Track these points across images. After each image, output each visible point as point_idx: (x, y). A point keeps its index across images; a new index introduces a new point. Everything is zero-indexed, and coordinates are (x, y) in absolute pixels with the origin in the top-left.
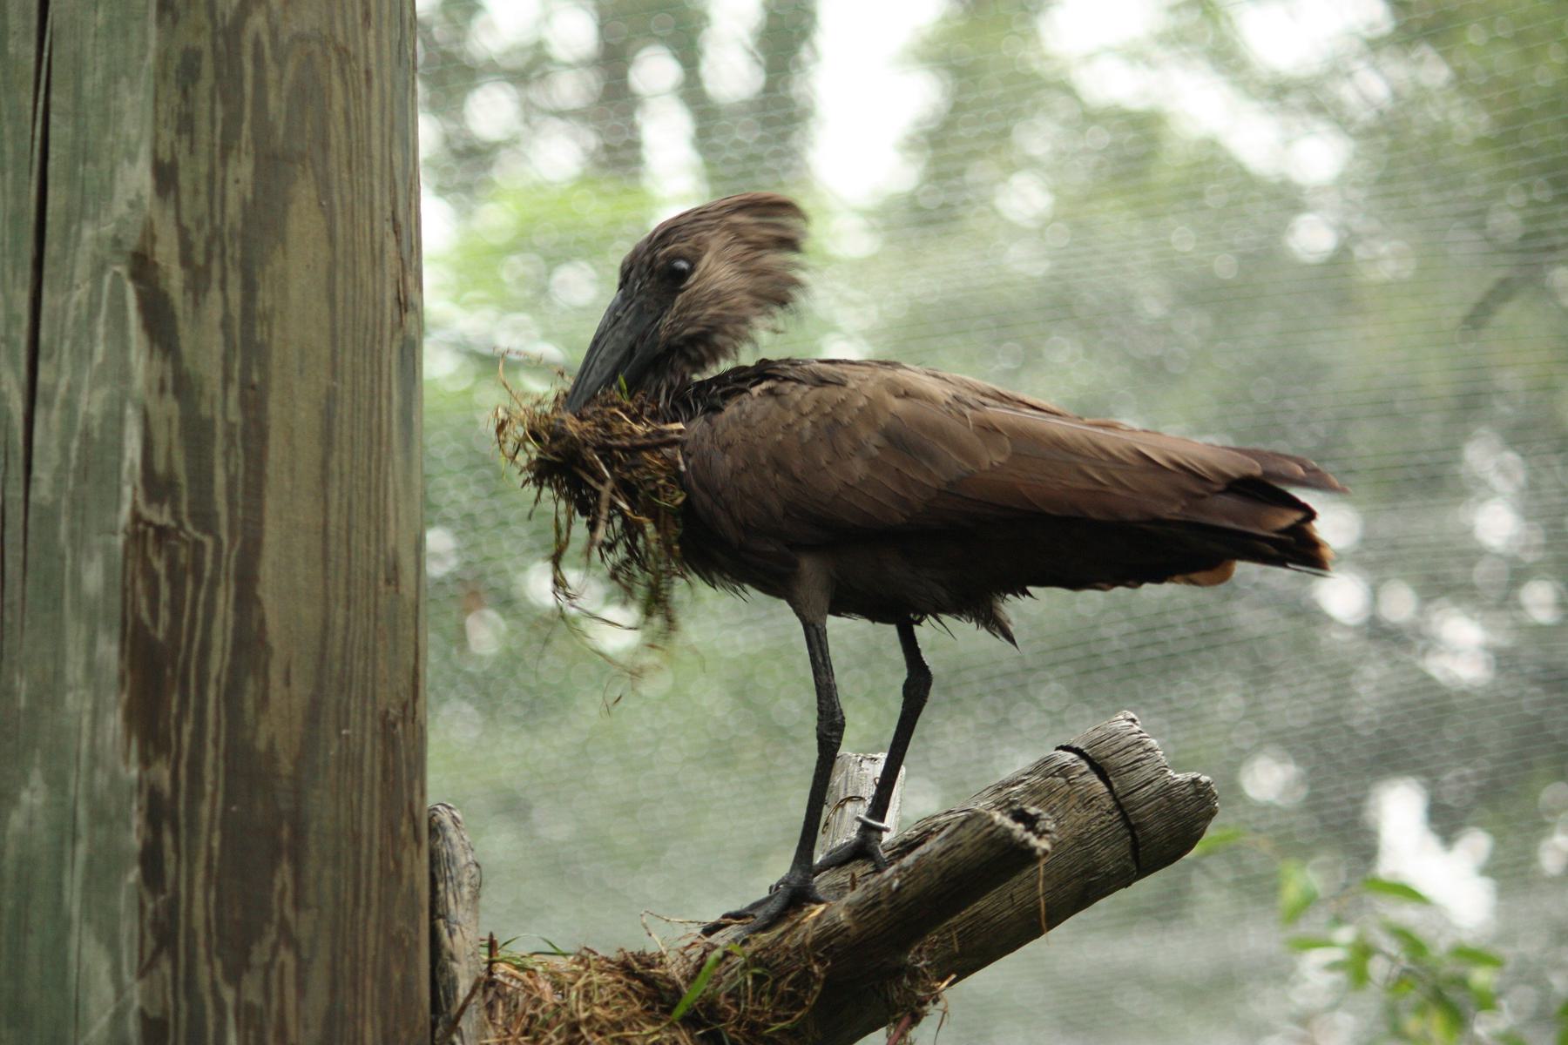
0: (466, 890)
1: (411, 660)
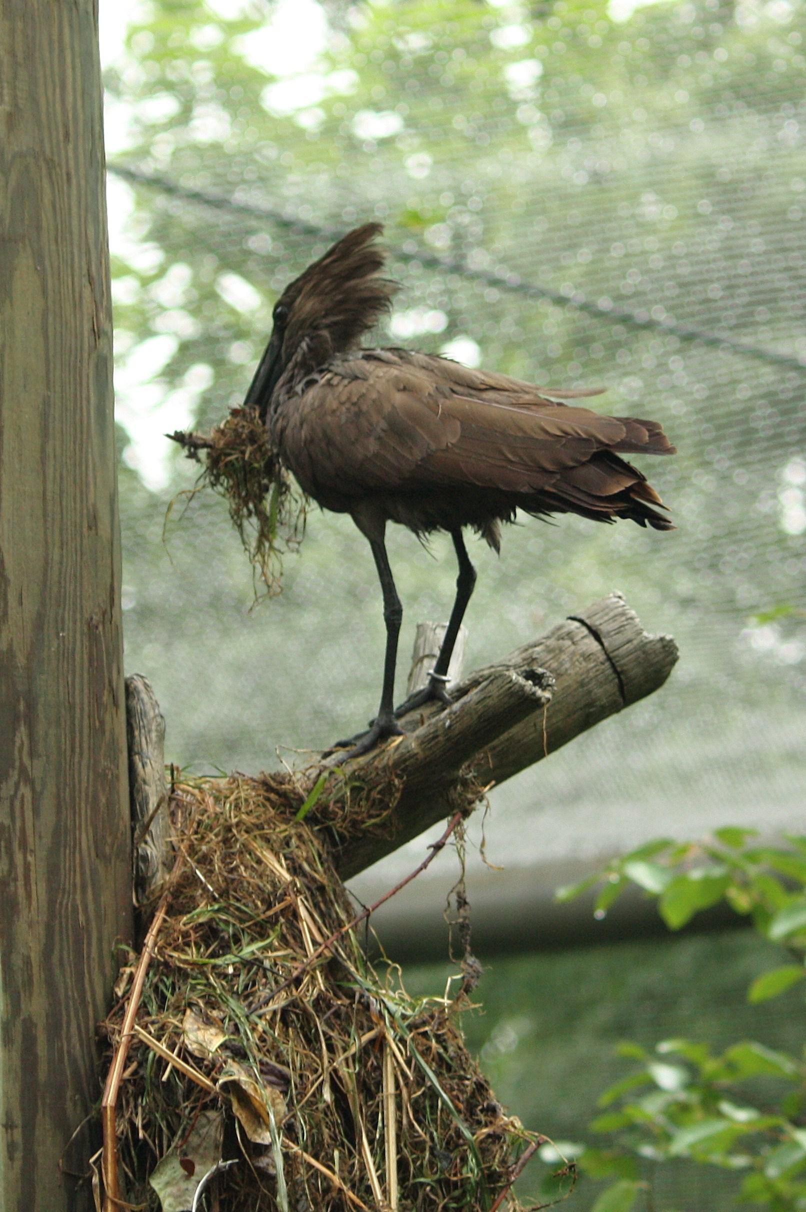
0: (154, 735)
1: (109, 581)
